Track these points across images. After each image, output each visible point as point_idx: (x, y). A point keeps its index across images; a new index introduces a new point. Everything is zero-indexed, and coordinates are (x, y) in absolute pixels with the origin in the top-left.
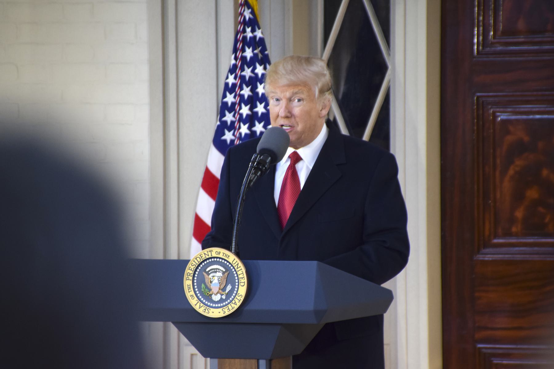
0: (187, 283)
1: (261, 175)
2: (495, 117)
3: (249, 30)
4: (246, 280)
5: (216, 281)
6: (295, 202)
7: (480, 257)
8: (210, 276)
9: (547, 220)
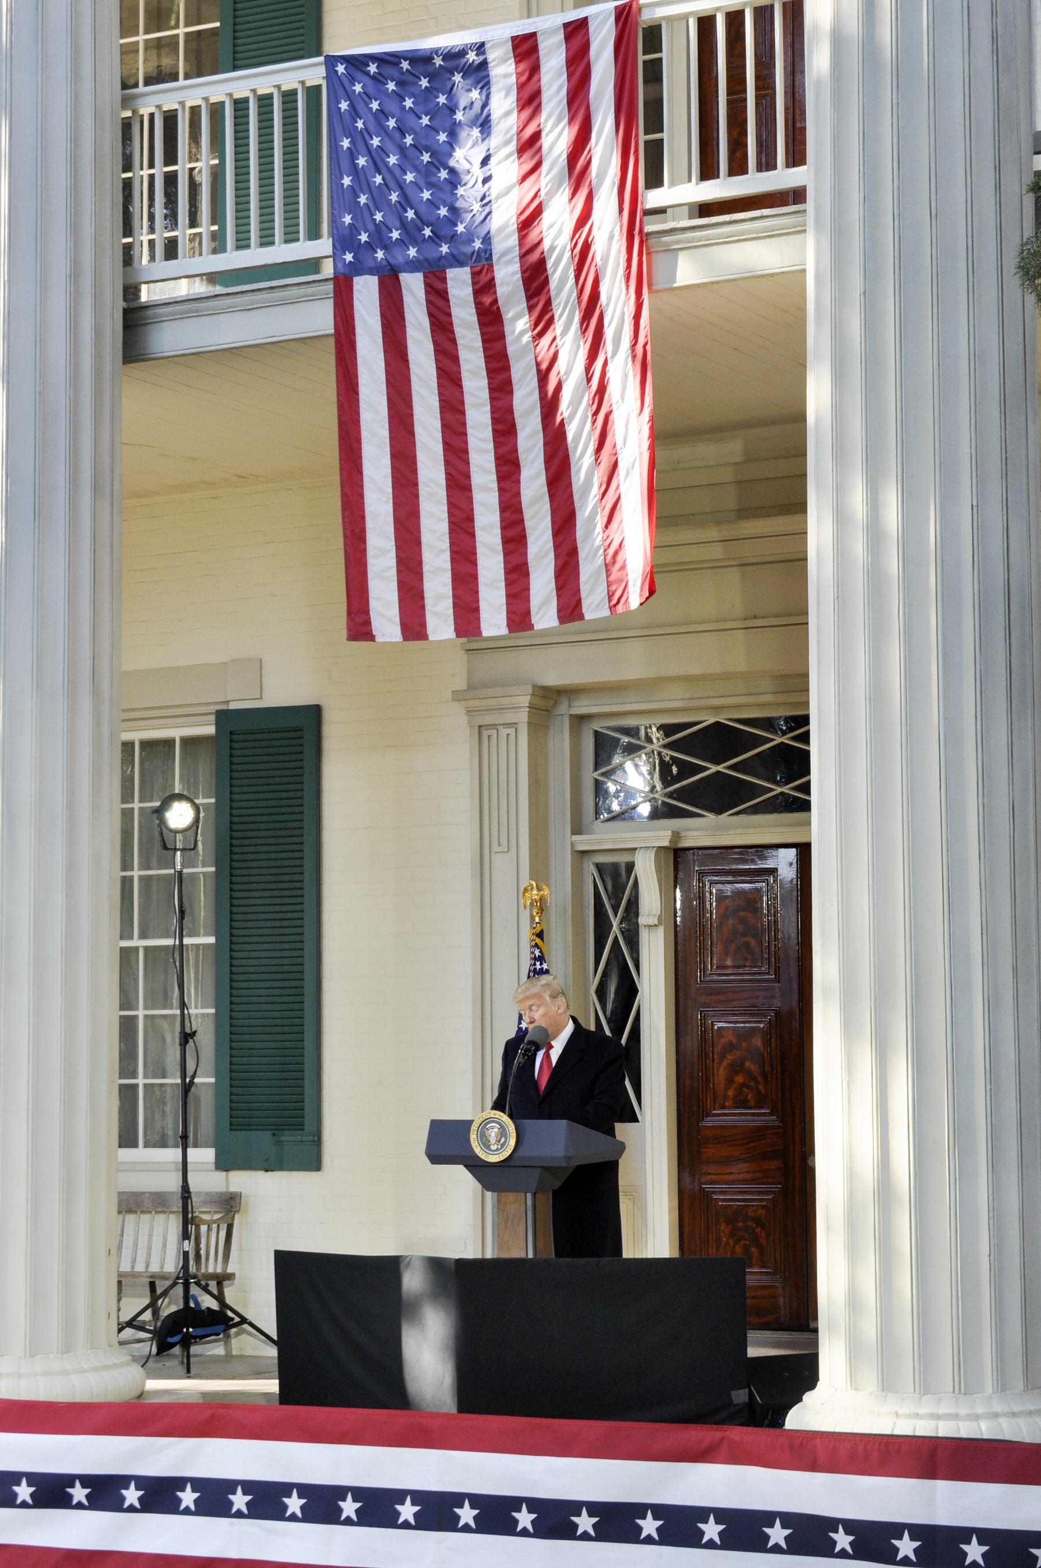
0: (473, 1137)
1: (527, 1059)
2: (713, 1025)
3: (538, 963)
4: (515, 1135)
5: (493, 1135)
6: (549, 1074)
7: (704, 1124)
8: (490, 1131)
9: (749, 1098)
